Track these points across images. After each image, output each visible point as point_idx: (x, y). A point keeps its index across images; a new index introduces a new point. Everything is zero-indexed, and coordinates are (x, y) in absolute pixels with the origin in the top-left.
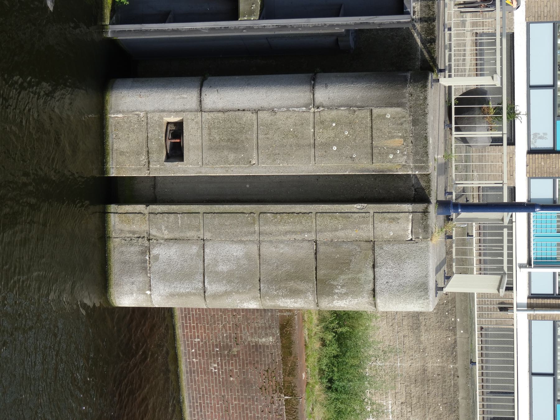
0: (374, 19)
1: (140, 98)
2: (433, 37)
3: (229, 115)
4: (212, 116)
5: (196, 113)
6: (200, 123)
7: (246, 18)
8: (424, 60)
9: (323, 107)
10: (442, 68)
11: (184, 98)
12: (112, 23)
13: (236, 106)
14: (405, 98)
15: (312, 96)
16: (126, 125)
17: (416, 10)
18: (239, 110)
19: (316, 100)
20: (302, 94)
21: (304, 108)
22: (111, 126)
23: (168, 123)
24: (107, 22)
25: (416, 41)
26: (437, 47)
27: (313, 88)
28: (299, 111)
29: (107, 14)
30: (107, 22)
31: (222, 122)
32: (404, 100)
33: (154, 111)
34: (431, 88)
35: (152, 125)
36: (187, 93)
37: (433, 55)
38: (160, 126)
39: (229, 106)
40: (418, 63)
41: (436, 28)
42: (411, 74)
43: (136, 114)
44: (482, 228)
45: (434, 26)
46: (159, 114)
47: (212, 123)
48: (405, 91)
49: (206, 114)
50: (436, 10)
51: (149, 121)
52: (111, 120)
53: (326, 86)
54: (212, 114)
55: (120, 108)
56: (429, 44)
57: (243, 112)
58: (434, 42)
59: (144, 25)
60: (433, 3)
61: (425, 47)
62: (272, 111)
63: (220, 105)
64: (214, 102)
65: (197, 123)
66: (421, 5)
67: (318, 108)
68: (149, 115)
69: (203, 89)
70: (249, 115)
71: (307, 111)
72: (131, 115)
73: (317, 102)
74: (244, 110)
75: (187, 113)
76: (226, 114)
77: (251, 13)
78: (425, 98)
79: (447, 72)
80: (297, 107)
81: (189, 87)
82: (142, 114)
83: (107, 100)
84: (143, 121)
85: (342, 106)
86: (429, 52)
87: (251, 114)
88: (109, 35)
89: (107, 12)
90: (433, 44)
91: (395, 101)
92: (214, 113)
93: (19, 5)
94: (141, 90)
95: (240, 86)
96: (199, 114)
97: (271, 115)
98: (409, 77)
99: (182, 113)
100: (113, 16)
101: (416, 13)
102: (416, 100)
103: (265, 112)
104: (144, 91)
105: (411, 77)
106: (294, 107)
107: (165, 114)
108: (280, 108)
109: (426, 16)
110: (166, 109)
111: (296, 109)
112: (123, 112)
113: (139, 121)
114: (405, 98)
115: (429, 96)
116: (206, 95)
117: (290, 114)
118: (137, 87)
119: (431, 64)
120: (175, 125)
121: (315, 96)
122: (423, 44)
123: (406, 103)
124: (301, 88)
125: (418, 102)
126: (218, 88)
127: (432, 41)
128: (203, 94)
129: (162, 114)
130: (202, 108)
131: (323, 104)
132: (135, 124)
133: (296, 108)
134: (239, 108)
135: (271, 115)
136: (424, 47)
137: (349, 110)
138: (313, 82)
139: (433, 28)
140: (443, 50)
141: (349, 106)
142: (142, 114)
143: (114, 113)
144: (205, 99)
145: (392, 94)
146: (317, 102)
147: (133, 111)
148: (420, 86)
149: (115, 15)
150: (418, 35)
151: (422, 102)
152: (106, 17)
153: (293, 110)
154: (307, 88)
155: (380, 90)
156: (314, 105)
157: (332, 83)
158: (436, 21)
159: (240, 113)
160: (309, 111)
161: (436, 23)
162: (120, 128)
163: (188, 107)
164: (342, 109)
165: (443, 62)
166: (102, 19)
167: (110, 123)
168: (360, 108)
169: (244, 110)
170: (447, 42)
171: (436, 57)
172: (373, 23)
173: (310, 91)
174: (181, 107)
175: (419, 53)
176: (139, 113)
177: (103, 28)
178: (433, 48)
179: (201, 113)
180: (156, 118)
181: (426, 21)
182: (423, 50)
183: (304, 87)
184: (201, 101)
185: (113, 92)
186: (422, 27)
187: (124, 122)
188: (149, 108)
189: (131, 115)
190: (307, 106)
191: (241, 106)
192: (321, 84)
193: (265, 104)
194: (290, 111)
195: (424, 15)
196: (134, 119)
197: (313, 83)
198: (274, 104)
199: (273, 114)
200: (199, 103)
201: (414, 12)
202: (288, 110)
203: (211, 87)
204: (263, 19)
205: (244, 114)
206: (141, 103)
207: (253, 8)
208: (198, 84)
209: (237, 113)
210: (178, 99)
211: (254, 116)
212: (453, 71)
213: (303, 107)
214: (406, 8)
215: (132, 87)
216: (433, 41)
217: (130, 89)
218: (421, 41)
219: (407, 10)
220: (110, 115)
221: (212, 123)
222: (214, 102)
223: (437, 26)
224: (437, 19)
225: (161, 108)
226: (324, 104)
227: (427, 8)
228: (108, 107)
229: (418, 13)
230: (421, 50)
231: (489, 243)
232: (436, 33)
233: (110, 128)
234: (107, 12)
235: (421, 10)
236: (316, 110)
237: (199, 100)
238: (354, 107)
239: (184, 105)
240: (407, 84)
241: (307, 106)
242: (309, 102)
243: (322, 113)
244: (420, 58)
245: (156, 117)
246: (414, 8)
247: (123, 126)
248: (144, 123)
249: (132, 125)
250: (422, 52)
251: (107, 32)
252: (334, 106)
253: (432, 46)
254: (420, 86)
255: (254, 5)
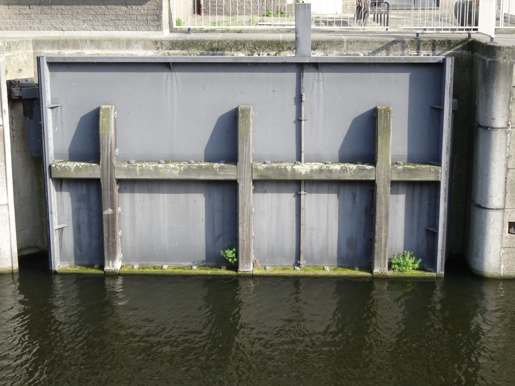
0: (448, 84)
1: (491, 253)
2: (447, 41)
3: (509, 189)
4: (508, 201)
5: (505, 213)
6: (512, 210)
7: (440, 176)
8: (463, 48)
9: (508, 121)
10: (468, 34)
11: (494, 221)
12: (435, 271)
13: (503, 184)
14: (506, 62)
15: (500, 129)
16: (510, 263)
17: (426, 54)
18: (506, 182)
19: (503, 126)
20: (498, 136)
21: (508, 135)
22: (509, 273)
23: (509, 232)
24: (434, 274)
25: (448, 54)
26: (453, 39)
27: (494, 128)
28: (510, 139)
29: (429, 275)
30: (434, 274)
31: (513, 194)
32: (508, 63)
33: (502, 243)
34: (497, 43)
35: (511, 244)
36: (490, 219)
37: (459, 42)
38: (512, 238)
39: (502, 189)
40: (465, 52)
41: (440, 39)
42: (488, 58)
43: (503, 255)
44: (423, 8)
45: (439, 41)
46: (503, 239)
47: (513, 201)
48: (502, 63)
49: (506, 205)
50: (427, 39)
51: (508, 246)
52: (505, 273)
53: (494, 119)
54: (507, 201)
55: (497, 266)
56: (451, 45)
57: (508, 179)
58: (450, 41)
59: (438, 248)
60: (422, 41)
61: (453, 47)
62: (508, 158)
63: (501, 195)
64: (499, 199)
65: (512, 212)
66: (423, 50)
67: (509, 125)
68: (504, 246)
69: (488, 207)
70: (510, 175)
71: (510, 133)
72: (503, 259)
73: (505, 125)
74: (506, 178)
75: (505, 219)
76: (508, 191)
77: (437, 172)
78: (508, 47)
79: (471, 32)
80: (507, 140)
81: (486, 217)
82: (503, 251)
83: (491, 276)
84: (507, 251)
85: (509, 108)
86: (457, 45)
87: (509, 173)
88: (443, 273)
89: (427, 274)
90: (451, 41)
91: (509, 69)
92: (506, 200)
93: (221, 334)
94: (485, 252)
95: (488, 181)
96: (506, 210)
97: (511, 159)
98: (491, 59)
99: (504, 222)
100: (428, 270)
101: (428, 53)
102: (509, 54)
103: (508, 163)
104: (486, 249)
105: (490, 58)
106: (507, 142)
107: (504, 235)
108: (506, 153)
109: (431, 46)
110: (501, 234)
111: (509, 141)
112: (500, 265)
113: (508, 253)
114: (506, 62)
115: (507, 45)
116: (493, 205)
117: (511, 146)
118: (483, 254)
119: (466, 43)
120: (511, 228)
121: (500, 127)
122: (451, 49)
123: (510, 61)
124: (493, 137)
125: (511, 53)
126: (489, 197)
127: (449, 42)
128: (492, 207)
129: (504, 237)
130: (502, 208)
131: (506, 122)
132: (509, 256)
133: (507, 141)
134: (504, 182)
135: (511, 159)
136: (453, 48)
137: (512, 103)
138: (489, 129)
139: (440, 41)
140: (440, 34)
141: (510, 103)
142: (503, 251)
143: (501, 271)
144: (496, 206)
145: (503, 71)
146: (505, 125)
147: (500, 257)
148: (499, 51)
149: (426, 268)
150: (444, 52)
151: (510, 50)
152: (431, 275)
153: (509, 143)
154: (494, 132)
155: (500, 80)
156: (506, 128)
157: (491, 115)
158: (435, 39)
159: (508, 181)
160: (511, 132)
161: (437, 39)
162: (511, 267)
163: (500, 218)
164: (511, 108)
165: (449, 35)
166: (433, 278)
167: (507, 274)
168: (512, 95)
169: (506, 178)
170: (435, 32)
171: (461, 39)
172: (450, 84)
173: (496, 130)
174: (500, 223)
175: (457, 52)
176: (502, 253)
177: (438, 278)
178: (454, 41)
179: (505, 209)
180: (506, 241)
181: (435, 47)
182: (455, 49)
183: (492, 135)
184: (497, 209)
185: (485, 271)
186: (439, 50)
187: (507, 264)
188: (499, 246)
189: (503, 259)
190: (507, 133)
191: (503, 180)
192: (492, 123)
193: (503, 163)
194: (509, 145)
195: (430, 48)
196: (506, 257)
197: (488, 129)
198: (503, 156)
199: (510, 157)
200: (498, 210)
201: (428, 55)
202: (509, 147)
203: (487, 202)
204: (99, 161)
205: (509, 178)
206: (495, 252)
207: (433, 171)
208: (483, 211)
209: (507, 184)
210: (494, 225)
211: (511, 171)
212: (455, 27)
213: (507, 136)
214: (440, 61)
215: (482, 258)
216: (449, 42)
217: (483, 259)
218: (449, 50)
219: (441, 60)
220: (502, 274)
221: (513, 201)
222: (499, 199)
223: (438, 39)
224: (433, 39)
225: (500, 237)
226: (506, 120)
227: (426, 45)
228: (496, 275)
229: (429, 52)
230: (455, 50)
231: (411, 2)
232: (443, 39)
233: (511, 274)
234: (427, 274)
235: (426, 50)
236: (510, 126)
237: (496, 210)
238: (510, 99)
239: (499, 221)
240: (496, 61)
241: (507, 133)
242: (504, 131)
243: (513, 122)
244: (460, 51)
245: (505, 241)
246: (424, 55)
247: (510, 265)
248: (509, 250)
249: (510, 258)
250: (456, 50)
251: (441, 274)
252: (508, 113)
253: (453, 42)
254: (499, 51)
255: (432, 170)
